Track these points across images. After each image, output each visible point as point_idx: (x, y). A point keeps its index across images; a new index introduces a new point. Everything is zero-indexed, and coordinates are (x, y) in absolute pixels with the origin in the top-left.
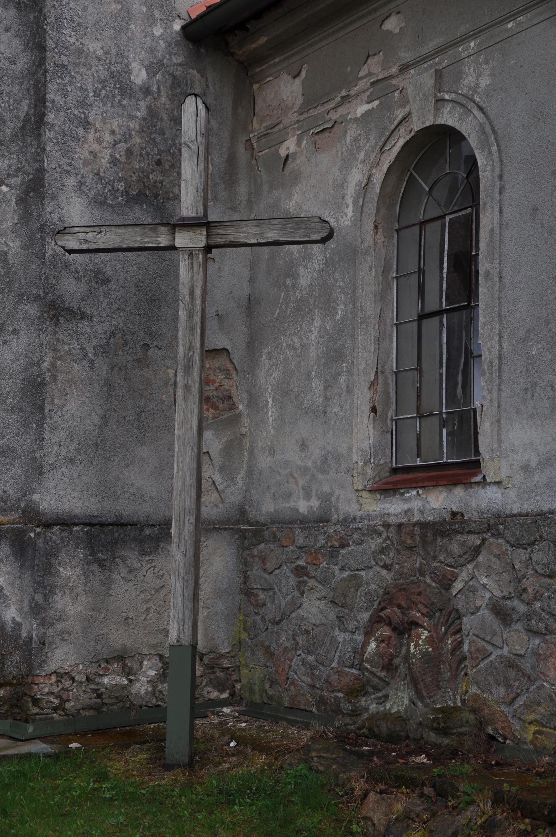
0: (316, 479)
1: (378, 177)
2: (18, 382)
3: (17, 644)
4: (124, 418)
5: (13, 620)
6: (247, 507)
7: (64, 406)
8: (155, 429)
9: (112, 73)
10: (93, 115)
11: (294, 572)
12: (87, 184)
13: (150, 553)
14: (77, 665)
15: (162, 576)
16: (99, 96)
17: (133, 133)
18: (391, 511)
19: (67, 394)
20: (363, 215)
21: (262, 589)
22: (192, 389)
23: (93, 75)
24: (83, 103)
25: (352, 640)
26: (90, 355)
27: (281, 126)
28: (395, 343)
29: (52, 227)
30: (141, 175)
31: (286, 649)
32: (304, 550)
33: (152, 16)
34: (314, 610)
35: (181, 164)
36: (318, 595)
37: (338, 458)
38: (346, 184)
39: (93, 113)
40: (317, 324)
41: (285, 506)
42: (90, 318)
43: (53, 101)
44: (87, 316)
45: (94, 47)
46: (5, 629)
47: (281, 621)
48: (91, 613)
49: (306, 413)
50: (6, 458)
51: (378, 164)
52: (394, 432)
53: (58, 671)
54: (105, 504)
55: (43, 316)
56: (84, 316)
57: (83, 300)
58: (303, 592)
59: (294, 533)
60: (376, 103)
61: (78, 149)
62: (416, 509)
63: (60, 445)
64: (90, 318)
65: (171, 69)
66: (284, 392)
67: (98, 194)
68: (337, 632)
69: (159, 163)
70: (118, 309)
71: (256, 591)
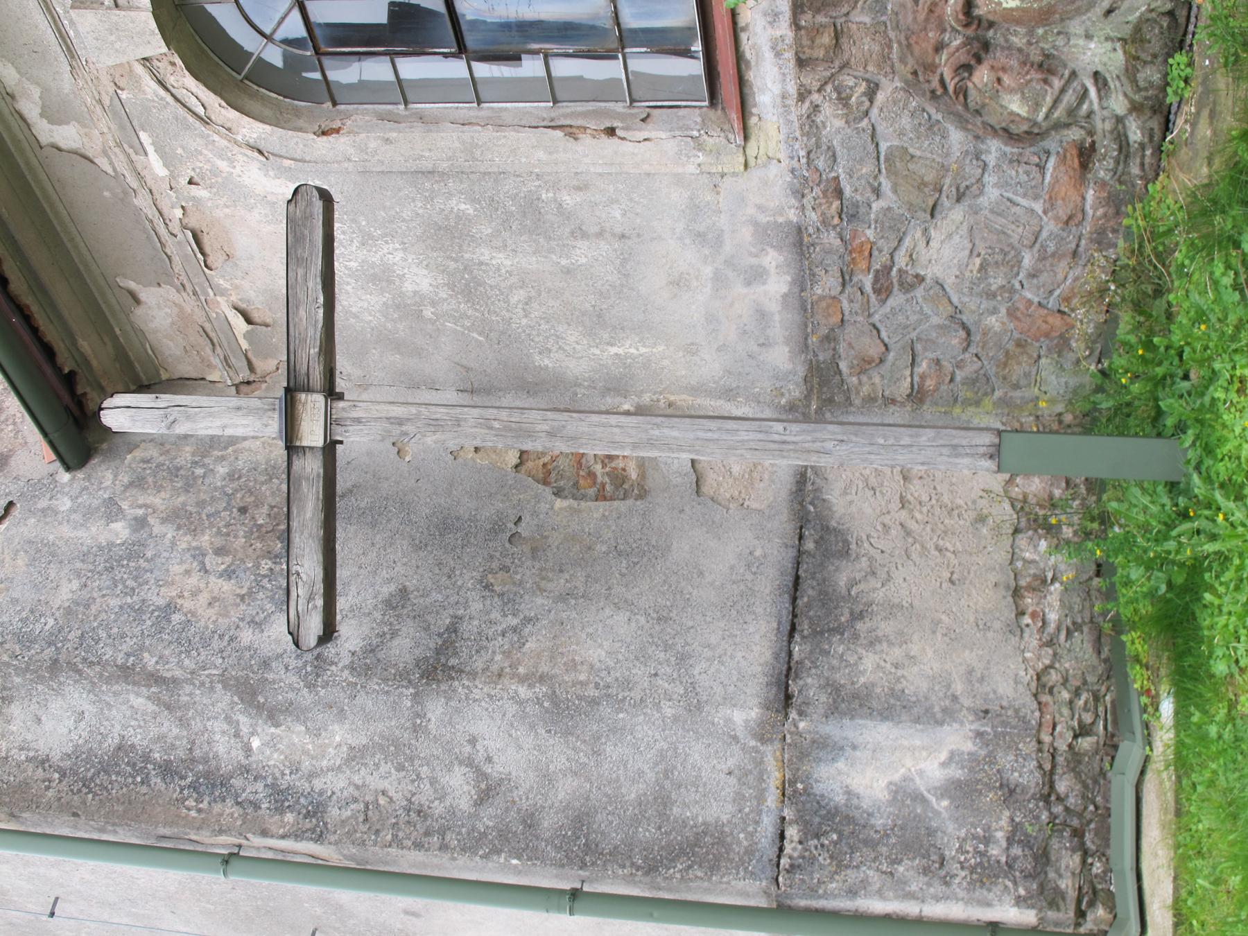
0: (733, 256)
1: (251, 130)
2: (551, 742)
3: (984, 759)
4: (623, 575)
5: (944, 765)
6: (783, 401)
7: (592, 667)
8: (646, 531)
9: (106, 569)
10: (158, 600)
11: (884, 296)
12: (254, 613)
13: (846, 543)
14: (1025, 660)
15: (884, 525)
16: (133, 589)
17: (194, 544)
18: (776, 89)
19: (573, 660)
20: (308, 159)
21: (913, 364)
22: (555, 424)
23: (104, 596)
24: (139, 611)
25: (998, 166)
26: (515, 622)
27: (208, 326)
28: (508, 105)
29: (309, 669)
30: (256, 535)
31: (1011, 313)
32: (847, 278)
33: (43, 510)
34: (947, 252)
35: (133, 392)
36: (922, 244)
37: (695, 209)
38: (269, 198)
39: (154, 598)
40: (484, 254)
41: (781, 325)
42: (457, 619)
43: (128, 655)
44: (452, 624)
45: (67, 591)
46: (959, 781)
47: (964, 326)
48: (939, 636)
49: (627, 276)
50: (675, 767)
51: (229, 130)
52: (652, 104)
53: (1034, 691)
54: (760, 610)
55: (445, 691)
56: (453, 629)
57: (427, 629)
58: (917, 276)
59: (822, 298)
60: (144, 136)
61: (202, 623)
62: (770, 31)
63: (656, 675)
64: (457, 619)
65: (119, 488)
66: (597, 323)
67: (272, 598)
68: (983, 201)
69: (243, 510)
70: (449, 577)
71: (916, 379)
